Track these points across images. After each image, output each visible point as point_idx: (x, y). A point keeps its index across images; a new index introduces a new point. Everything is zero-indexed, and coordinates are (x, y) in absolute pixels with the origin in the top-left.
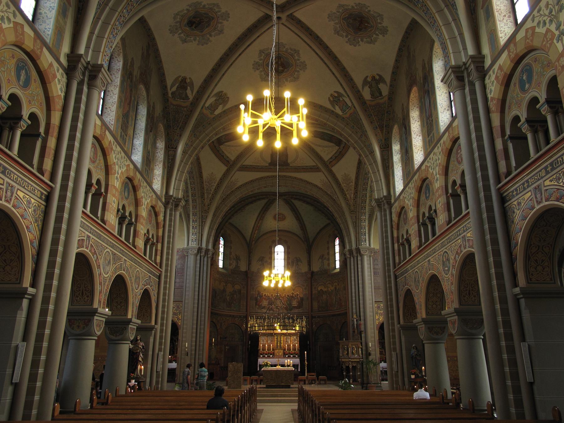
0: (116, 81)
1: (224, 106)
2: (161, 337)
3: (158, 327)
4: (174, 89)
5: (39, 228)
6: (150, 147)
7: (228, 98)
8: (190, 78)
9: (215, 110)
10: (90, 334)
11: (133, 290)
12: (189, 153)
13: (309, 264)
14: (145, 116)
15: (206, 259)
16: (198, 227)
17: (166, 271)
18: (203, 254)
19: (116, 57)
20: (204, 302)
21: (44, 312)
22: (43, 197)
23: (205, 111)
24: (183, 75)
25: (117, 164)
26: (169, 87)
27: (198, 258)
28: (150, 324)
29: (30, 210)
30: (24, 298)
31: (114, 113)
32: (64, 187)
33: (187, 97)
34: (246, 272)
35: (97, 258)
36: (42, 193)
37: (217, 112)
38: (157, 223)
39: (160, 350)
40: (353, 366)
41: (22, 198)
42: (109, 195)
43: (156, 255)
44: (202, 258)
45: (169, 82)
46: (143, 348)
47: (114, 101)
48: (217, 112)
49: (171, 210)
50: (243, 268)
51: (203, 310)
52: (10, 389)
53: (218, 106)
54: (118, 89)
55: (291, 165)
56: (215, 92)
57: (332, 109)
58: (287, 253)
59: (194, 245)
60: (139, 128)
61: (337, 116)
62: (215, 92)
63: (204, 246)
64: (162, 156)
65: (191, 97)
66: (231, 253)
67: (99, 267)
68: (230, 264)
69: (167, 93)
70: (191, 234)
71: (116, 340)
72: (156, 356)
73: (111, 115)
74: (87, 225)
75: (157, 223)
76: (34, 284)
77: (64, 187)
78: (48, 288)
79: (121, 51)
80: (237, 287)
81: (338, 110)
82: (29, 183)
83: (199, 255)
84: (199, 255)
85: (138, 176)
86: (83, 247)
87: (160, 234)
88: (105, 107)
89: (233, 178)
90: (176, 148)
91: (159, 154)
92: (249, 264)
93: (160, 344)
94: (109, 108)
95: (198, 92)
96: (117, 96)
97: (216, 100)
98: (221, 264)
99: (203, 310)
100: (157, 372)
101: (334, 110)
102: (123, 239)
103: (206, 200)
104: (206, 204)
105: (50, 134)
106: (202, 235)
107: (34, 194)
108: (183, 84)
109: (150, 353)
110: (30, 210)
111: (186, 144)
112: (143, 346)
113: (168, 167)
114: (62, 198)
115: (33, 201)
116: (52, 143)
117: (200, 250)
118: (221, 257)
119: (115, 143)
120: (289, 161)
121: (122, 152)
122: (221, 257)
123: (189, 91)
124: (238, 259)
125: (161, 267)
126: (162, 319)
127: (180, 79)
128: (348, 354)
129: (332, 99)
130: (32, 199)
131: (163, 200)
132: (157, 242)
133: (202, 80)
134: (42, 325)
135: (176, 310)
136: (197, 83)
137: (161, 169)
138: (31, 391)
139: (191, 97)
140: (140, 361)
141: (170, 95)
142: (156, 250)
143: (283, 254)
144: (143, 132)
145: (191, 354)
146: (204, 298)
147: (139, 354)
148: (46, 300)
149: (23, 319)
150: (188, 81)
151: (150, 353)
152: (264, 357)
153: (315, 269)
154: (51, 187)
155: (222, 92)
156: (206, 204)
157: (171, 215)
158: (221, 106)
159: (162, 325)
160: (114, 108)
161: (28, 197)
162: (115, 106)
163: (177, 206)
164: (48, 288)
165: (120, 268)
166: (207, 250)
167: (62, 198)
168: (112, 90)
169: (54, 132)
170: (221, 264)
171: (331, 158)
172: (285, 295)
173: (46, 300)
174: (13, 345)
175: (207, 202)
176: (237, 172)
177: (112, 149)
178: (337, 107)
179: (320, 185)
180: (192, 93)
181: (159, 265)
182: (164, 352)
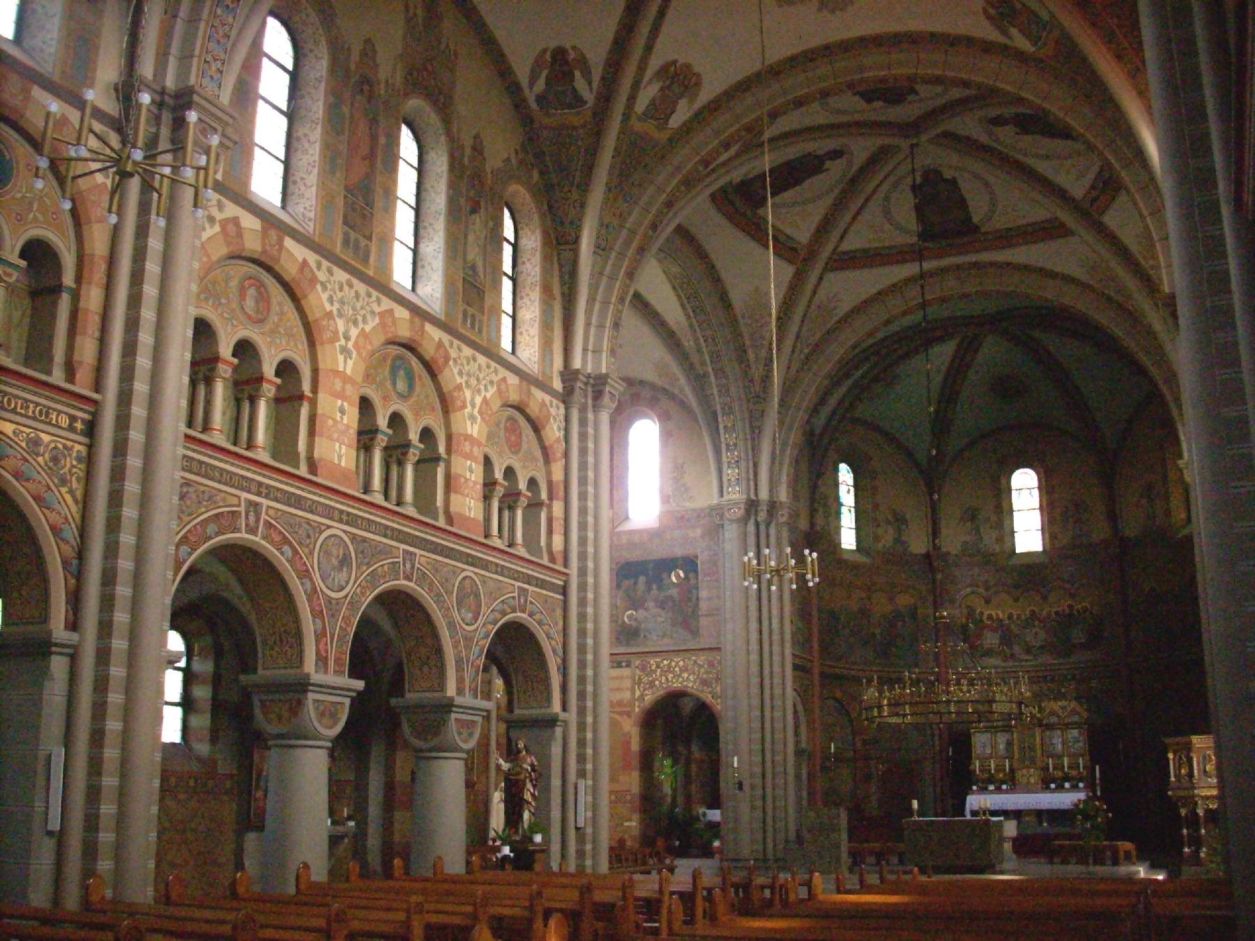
0: (314, 109)
1: (692, 100)
2: (582, 743)
3: (572, 716)
4: (540, 85)
5: (74, 497)
6: (473, 254)
7: (698, 75)
8: (574, 48)
9: (668, 117)
10: (304, 735)
11: (451, 625)
12: (617, 248)
13: (1113, 517)
14: (445, 175)
15: (772, 531)
16: (741, 444)
17: (583, 572)
18: (762, 516)
19: (311, 51)
20: (776, 649)
21: (101, 685)
22: (79, 425)
23: (638, 126)
24: (553, 45)
25: (341, 315)
26: (524, 82)
27: (751, 528)
28: (548, 711)
29: (40, 459)
30: (51, 653)
31: (314, 189)
32: (125, 398)
33: (580, 101)
34: (927, 556)
35: (295, 552)
36: (73, 419)
37: (676, 121)
38: (545, 450)
39: (582, 774)
40: (1208, 811)
41: (11, 435)
42: (321, 396)
43: (550, 532)
44: (762, 527)
45: (522, 73)
46: (533, 770)
47: (311, 160)
48: (676, 121)
49: (583, 410)
50: (918, 544)
51: (777, 669)
52: (49, 845)
53: (675, 103)
54: (319, 128)
55: (983, 230)
56: (655, 64)
57: (1001, 39)
58: (1046, 488)
59: (736, 494)
60: (433, 208)
61: (1021, 56)
62: (655, 64)
63: (764, 495)
64: (538, 269)
65: (589, 97)
66: (876, 506)
67: (305, 574)
68: (877, 539)
69: (524, 100)
70: (725, 466)
71: (430, 750)
72: (571, 790)
73: (307, 195)
74: (212, 479)
75: (545, 450)
76: (74, 625)
77: (125, 398)
78: (105, 628)
79: (321, 31)
80: (904, 600)
81: (1021, 42)
82: (26, 400)
83: (752, 521)
84: (752, 521)
85: (434, 333)
86: (239, 531)
87: (558, 475)
88: (291, 179)
89: (821, 294)
90: (577, 241)
91: (528, 265)
92: (935, 533)
93: (581, 759)
94: (302, 179)
95: (603, 78)
96: (317, 146)
97: (662, 89)
98: (848, 540)
99: (777, 669)
100: (577, 829)
101: (1009, 42)
102: (378, 499)
103: (753, 367)
104: (757, 377)
105: (84, 281)
106: (756, 465)
107: (50, 423)
108: (561, 64)
109: (556, 782)
110: (40, 459)
111: (603, 225)
112: (532, 766)
113: (563, 294)
114: (123, 422)
115: (46, 438)
116: (93, 298)
117: (752, 506)
118: (848, 520)
119: (325, 264)
120: (975, 220)
121: (355, 281)
122: (848, 520)
123: (580, 83)
124: (900, 520)
125: (566, 563)
126: (582, 695)
127: (548, 57)
128: (1191, 775)
129: (992, 12)
130: (42, 435)
131: (557, 385)
132: (551, 498)
133: (607, 46)
134: (99, 710)
135: (707, 673)
136: (597, 55)
137: (537, 304)
138: (90, 851)
139: (589, 97)
140: (528, 803)
141: (534, 105)
142: (550, 520)
143: (1036, 493)
144: (442, 219)
145: (753, 787)
146: (776, 637)
147: (525, 785)
148: (103, 655)
149: (59, 698)
150: (572, 55)
151: (556, 782)
152: (983, 790)
153: (1131, 530)
154: (95, 402)
155: (674, 62)
156: (757, 377)
157: (583, 423)
158: (683, 104)
159: (582, 711)
160: (313, 179)
161: (28, 430)
162: (316, 171)
163: (598, 395)
164: (105, 628)
165: (394, 570)
166: (773, 506)
167: (123, 422)
168: (305, 135)
169: (98, 273)
170: (848, 540)
171: (1093, 187)
172: (1049, 614)
173: (103, 655)
174: (42, 754)
175: (757, 372)
176: (830, 276)
177: (313, 280)
178: (1014, 31)
179: (1079, 273)
180: (590, 84)
181: (560, 558)
182: (595, 779)
